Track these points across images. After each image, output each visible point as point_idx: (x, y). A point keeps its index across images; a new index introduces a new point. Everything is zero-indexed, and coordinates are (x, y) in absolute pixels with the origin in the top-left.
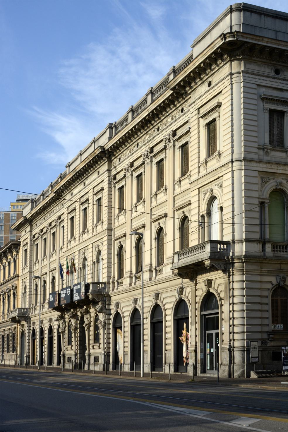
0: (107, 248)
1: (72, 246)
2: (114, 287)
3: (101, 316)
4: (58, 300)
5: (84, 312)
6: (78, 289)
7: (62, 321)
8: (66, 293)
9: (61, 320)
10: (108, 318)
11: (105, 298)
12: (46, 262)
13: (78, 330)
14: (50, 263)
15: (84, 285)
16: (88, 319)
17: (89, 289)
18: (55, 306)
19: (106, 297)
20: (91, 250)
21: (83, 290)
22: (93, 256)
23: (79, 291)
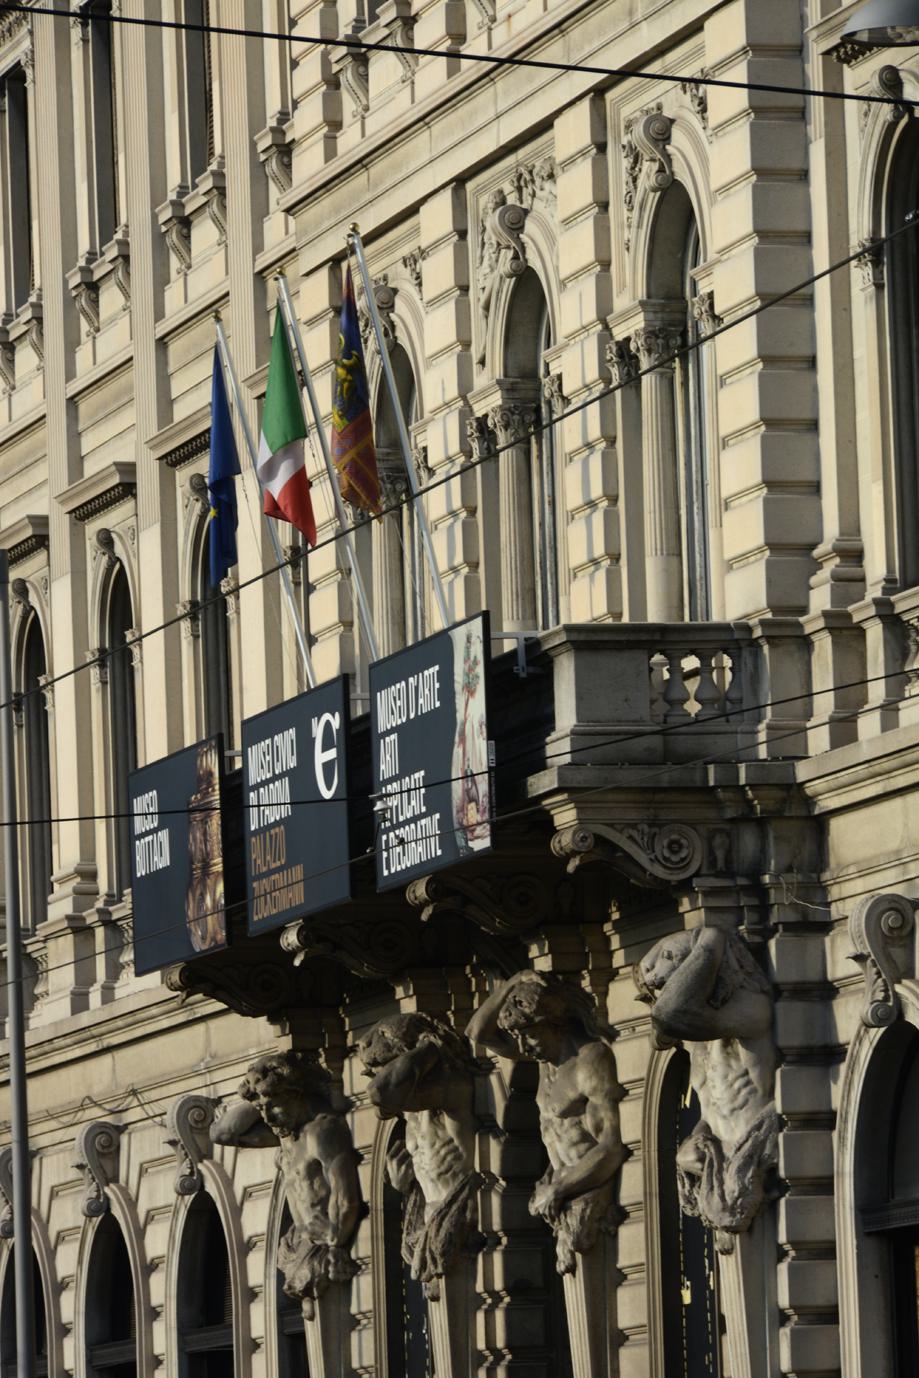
0: (744, 162)
1: (381, 124)
2: (851, 691)
3: (717, 1079)
4: (218, 865)
5: (527, 1026)
6: (422, 719)
7: (311, 1146)
8: (301, 776)
9: (296, 1132)
10: (805, 1105)
11: (748, 842)
12: (119, 332)
13: (493, 1270)
14: (162, 343)
15: (480, 670)
16: (588, 1122)
17: (548, 722)
18: (199, 946)
19: (761, 823)
20: (576, 187)
21: (474, 751)
22: (606, 265)
23: (429, 739)
